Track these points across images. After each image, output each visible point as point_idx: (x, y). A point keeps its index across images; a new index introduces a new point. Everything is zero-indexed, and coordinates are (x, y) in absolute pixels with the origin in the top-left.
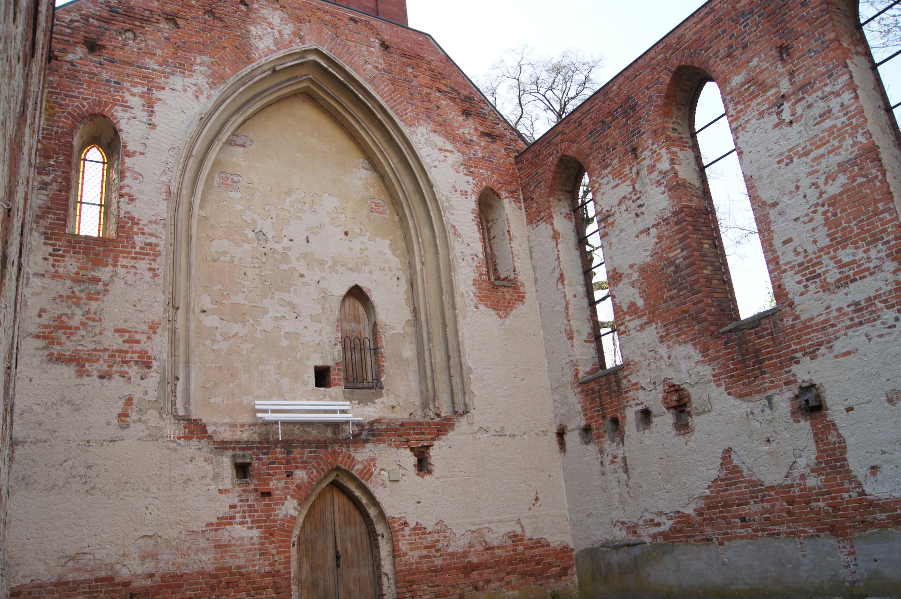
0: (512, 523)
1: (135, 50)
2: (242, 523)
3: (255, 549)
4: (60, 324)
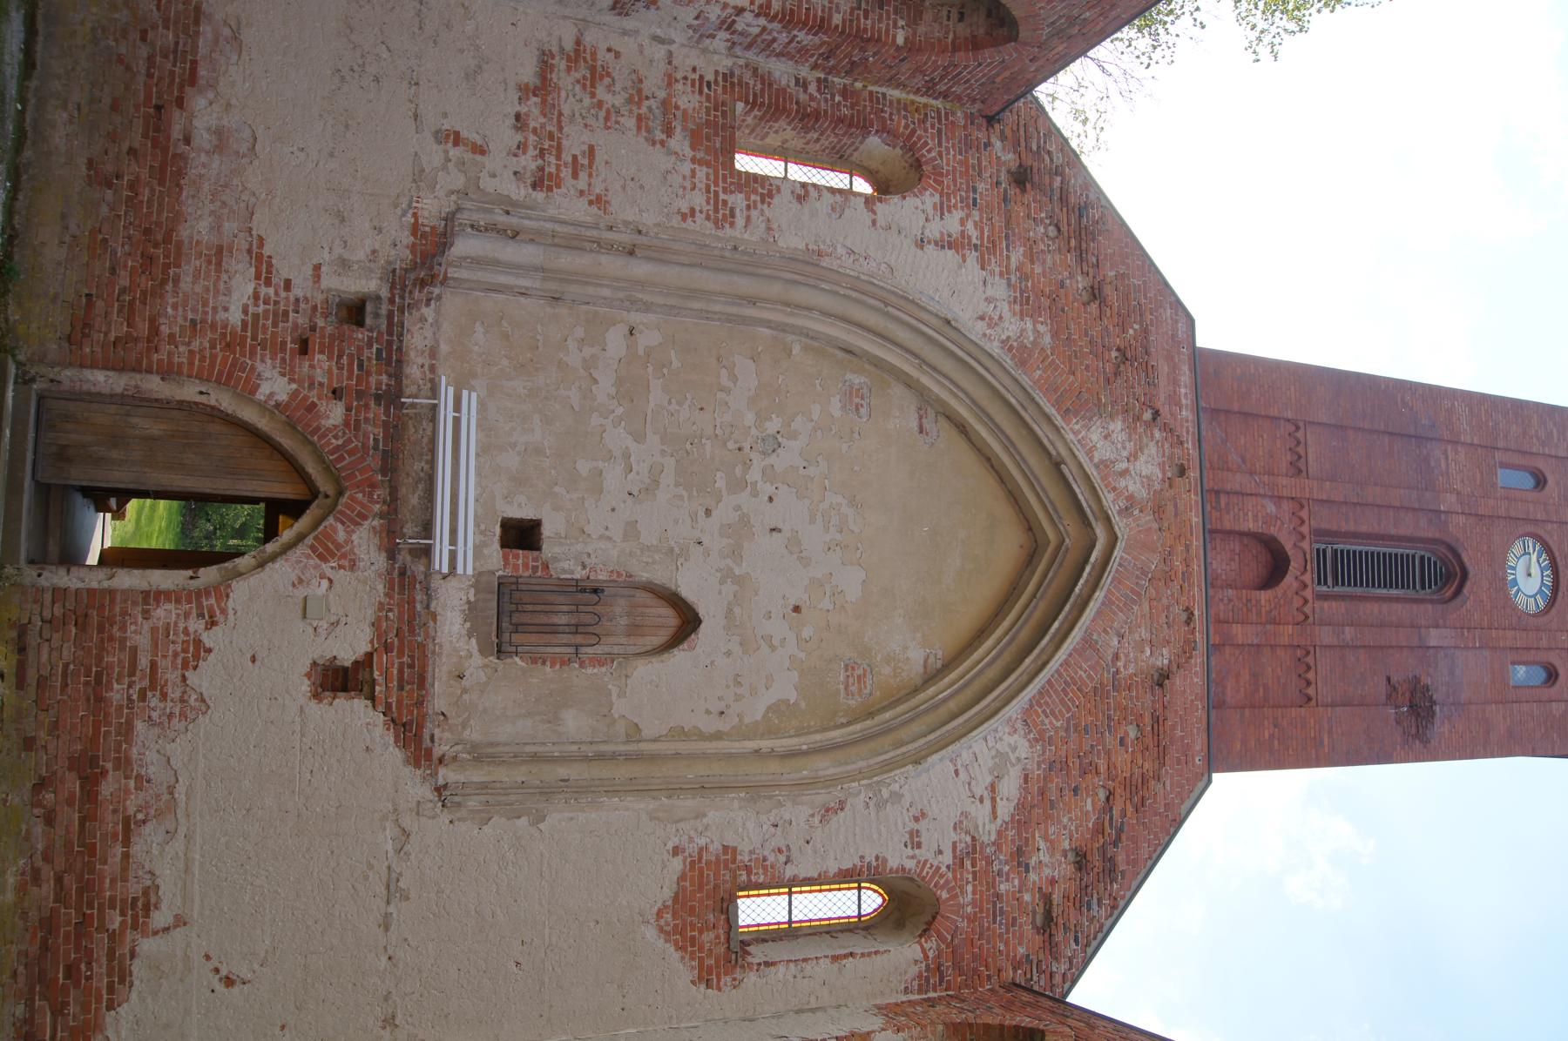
1: (1031, 233)
2: (256, 296)
3: (206, 313)
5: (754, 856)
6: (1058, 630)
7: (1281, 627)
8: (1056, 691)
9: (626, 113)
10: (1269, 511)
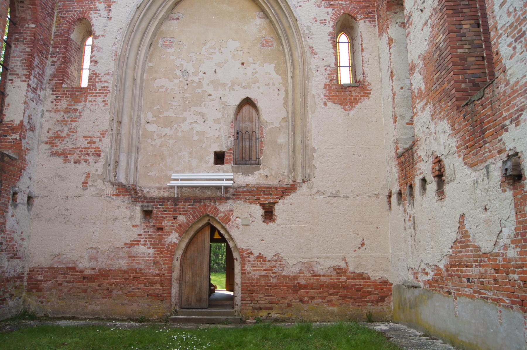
0: (338, 260)
2: (144, 245)
3: (151, 260)
4: (58, 136)
5: (328, 78)
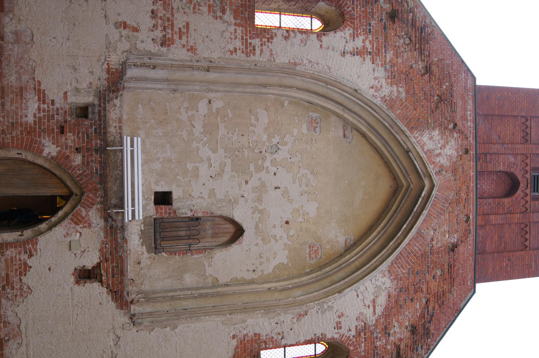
1: (397, 44)
2: (39, 109)
3: (17, 119)
6: (406, 228)
7: (514, 215)
8: (404, 257)
9: (203, 4)
10: (511, 161)
